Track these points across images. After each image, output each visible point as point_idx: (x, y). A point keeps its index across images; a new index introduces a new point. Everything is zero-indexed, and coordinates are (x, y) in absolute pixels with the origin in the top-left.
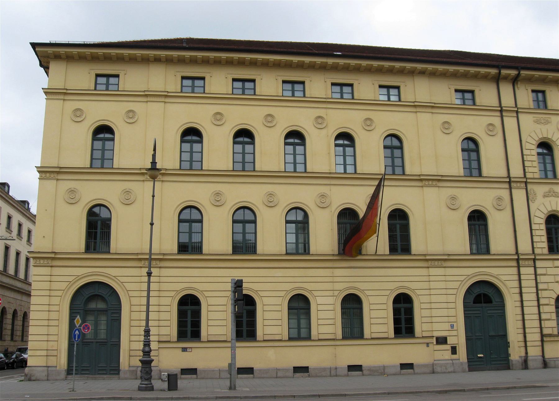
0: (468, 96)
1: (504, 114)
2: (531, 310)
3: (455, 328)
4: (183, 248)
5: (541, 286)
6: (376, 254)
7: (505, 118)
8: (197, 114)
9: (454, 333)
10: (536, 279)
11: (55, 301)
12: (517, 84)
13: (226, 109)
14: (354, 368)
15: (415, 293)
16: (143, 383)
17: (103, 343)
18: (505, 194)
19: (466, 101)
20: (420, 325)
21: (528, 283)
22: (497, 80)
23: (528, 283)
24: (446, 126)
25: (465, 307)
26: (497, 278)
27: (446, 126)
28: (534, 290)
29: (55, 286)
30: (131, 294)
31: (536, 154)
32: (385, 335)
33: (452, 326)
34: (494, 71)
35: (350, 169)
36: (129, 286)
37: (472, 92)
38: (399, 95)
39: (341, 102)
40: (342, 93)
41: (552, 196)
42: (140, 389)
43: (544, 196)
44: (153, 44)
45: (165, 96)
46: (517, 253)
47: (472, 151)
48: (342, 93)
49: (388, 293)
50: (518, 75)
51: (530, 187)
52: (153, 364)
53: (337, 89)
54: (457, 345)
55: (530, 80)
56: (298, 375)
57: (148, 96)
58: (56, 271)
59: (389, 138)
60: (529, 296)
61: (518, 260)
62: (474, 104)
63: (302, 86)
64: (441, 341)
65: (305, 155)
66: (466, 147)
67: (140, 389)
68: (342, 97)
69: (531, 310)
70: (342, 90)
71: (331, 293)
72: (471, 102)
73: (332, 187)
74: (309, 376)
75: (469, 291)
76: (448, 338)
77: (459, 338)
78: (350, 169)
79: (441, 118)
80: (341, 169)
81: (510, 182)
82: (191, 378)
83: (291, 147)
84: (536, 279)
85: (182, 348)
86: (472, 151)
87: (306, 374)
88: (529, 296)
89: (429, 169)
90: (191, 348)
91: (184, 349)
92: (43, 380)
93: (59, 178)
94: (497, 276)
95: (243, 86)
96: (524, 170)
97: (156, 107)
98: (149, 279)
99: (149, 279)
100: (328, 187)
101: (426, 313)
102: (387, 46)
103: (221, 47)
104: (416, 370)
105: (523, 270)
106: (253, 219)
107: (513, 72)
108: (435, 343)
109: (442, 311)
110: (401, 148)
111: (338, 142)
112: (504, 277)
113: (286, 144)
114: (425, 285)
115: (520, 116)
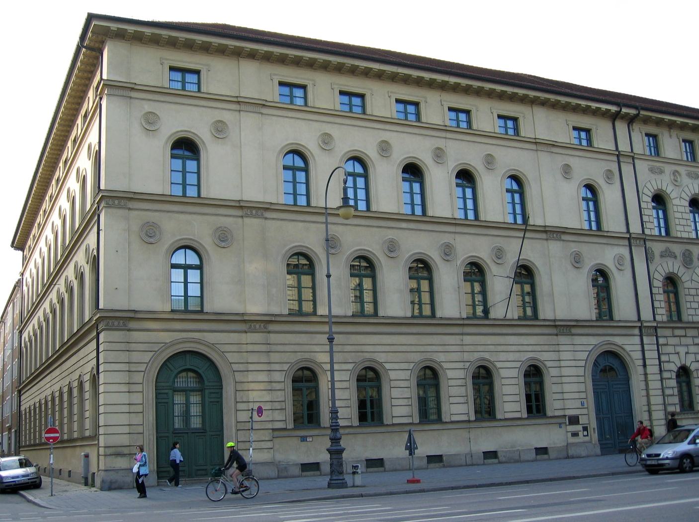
0: (356, 101)
1: (621, 159)
2: (655, 384)
3: (586, 406)
4: (600, 317)
5: (663, 358)
6: (201, 311)
7: (622, 164)
8: (305, 134)
9: (585, 411)
10: (658, 350)
11: (138, 378)
12: (632, 125)
13: (335, 131)
14: (491, 455)
15: (441, 366)
16: (334, 478)
17: (202, 432)
18: (625, 252)
19: (354, 108)
20: (553, 405)
21: (651, 355)
22: (614, 117)
23: (651, 355)
24: (567, 171)
25: (593, 381)
26: (622, 348)
27: (567, 171)
28: (657, 362)
29: (135, 357)
30: (235, 367)
31: (651, 207)
32: (518, 415)
33: (582, 404)
34: (614, 109)
35: (302, 201)
36: (232, 358)
37: (416, 104)
38: (305, 98)
39: (181, 95)
40: (184, 83)
41: (669, 256)
42: (330, 486)
43: (662, 256)
44: (216, 30)
45: (260, 106)
46: (639, 320)
47: (360, 175)
48: (184, 83)
49: (350, 366)
50: (638, 115)
51: (648, 244)
52: (344, 455)
53: (178, 76)
54: (588, 425)
55: (646, 121)
56: (432, 465)
57: (240, 103)
58: (273, 338)
59: (291, 156)
60: (653, 369)
61: (642, 329)
62: (364, 113)
63: (196, 76)
64: (574, 420)
65: (198, 173)
66: (290, 164)
67: (330, 486)
68: (184, 89)
69: (655, 384)
70: (184, 78)
71: (460, 365)
72: (359, 110)
73: (457, 236)
74: (444, 466)
75: (596, 364)
76: (580, 416)
77: (589, 418)
78: (192, 192)
79: (560, 160)
80: (178, 190)
81: (630, 239)
82: (314, 475)
83: (180, 162)
84: (658, 350)
85: (301, 437)
86: (360, 175)
87: (381, 469)
88: (653, 369)
89: (552, 221)
90: (312, 436)
91: (304, 439)
92: (478, 465)
93: (131, 206)
94: (624, 346)
95: (184, 78)
96: (642, 225)
97: (249, 120)
98: (331, 348)
99: (331, 348)
100: (453, 235)
101: (555, 388)
102: (501, 70)
103: (597, 97)
104: (552, 454)
105: (645, 339)
106: (197, 262)
107: (633, 112)
108: (568, 424)
109: (571, 387)
110: (306, 170)
111: (175, 152)
112: (629, 345)
113: (173, 157)
114: (553, 356)
115: (636, 161)
